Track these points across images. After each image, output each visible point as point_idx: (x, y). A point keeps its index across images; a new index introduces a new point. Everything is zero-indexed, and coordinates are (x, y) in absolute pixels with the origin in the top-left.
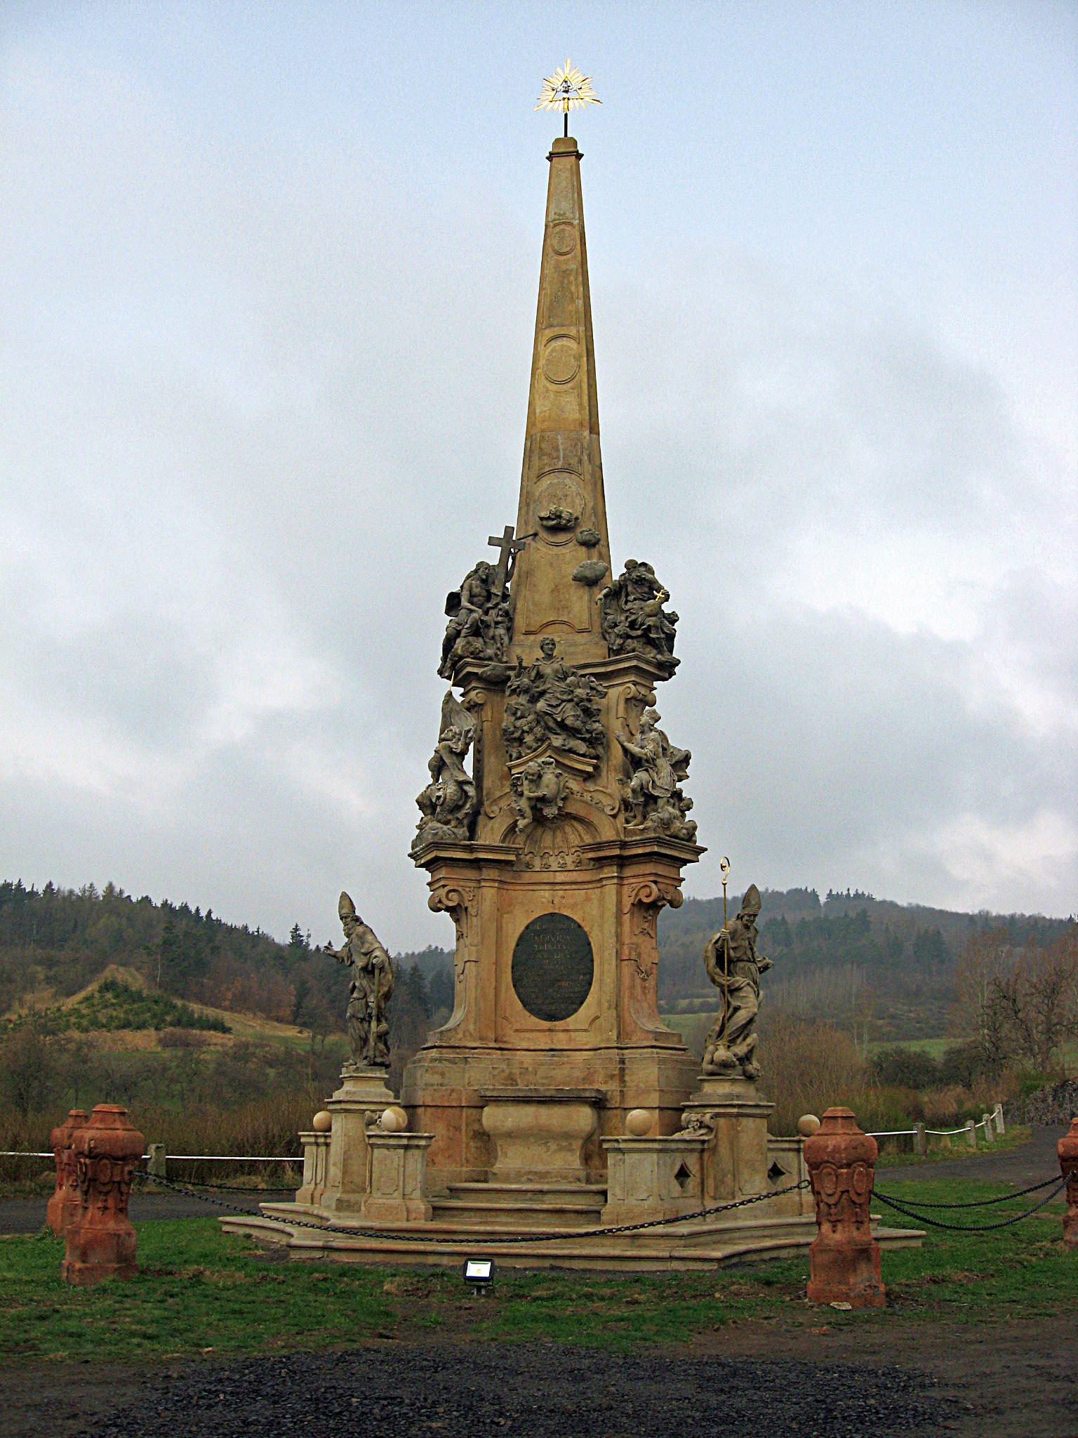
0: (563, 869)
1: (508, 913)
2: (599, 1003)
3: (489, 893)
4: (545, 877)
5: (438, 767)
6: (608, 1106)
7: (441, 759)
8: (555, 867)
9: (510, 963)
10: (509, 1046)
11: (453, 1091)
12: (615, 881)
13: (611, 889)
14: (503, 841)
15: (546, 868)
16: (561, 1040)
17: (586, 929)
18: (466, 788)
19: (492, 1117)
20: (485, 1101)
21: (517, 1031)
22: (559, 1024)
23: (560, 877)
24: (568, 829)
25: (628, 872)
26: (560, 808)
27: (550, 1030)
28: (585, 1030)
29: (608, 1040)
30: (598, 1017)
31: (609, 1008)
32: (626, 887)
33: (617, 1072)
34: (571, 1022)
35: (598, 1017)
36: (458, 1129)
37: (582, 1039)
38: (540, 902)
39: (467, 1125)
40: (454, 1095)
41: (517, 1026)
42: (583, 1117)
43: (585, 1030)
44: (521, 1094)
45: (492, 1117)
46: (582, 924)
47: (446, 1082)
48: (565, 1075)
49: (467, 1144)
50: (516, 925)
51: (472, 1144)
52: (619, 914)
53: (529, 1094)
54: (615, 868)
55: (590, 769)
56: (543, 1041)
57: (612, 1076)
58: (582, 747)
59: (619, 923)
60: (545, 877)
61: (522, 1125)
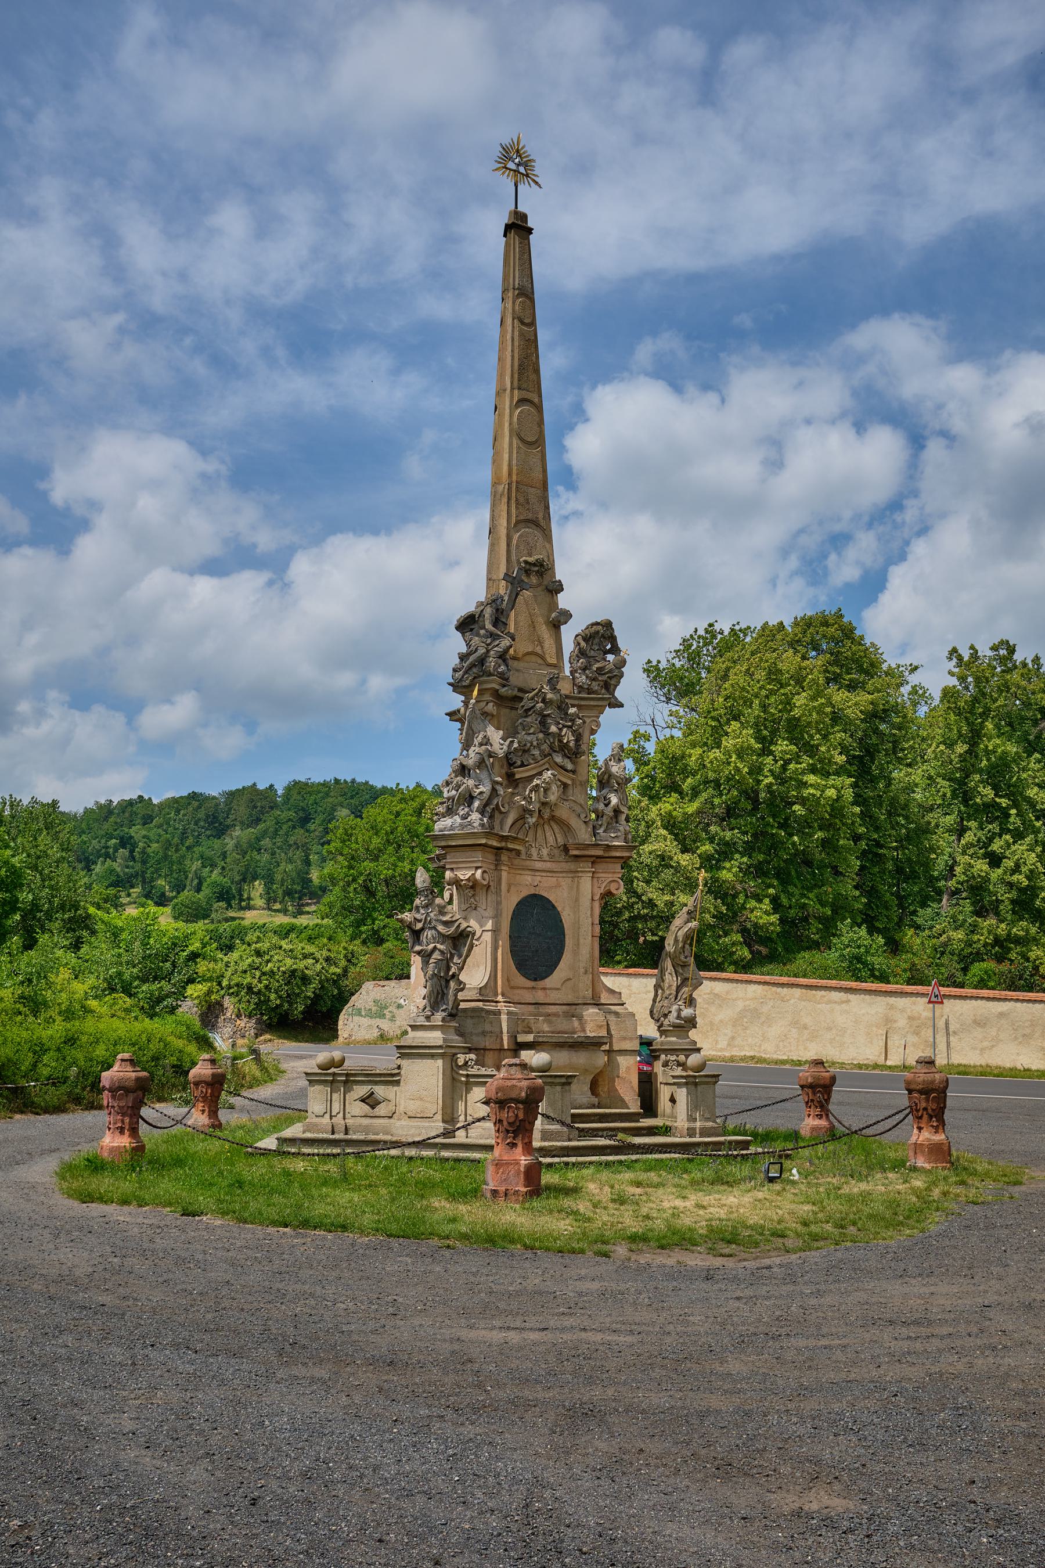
0: (541, 860)
16: (540, 996)
17: (559, 909)
22: (541, 984)
28: (558, 989)
34: (549, 982)
37: (553, 997)
56: (528, 997)
57: (601, 1027)
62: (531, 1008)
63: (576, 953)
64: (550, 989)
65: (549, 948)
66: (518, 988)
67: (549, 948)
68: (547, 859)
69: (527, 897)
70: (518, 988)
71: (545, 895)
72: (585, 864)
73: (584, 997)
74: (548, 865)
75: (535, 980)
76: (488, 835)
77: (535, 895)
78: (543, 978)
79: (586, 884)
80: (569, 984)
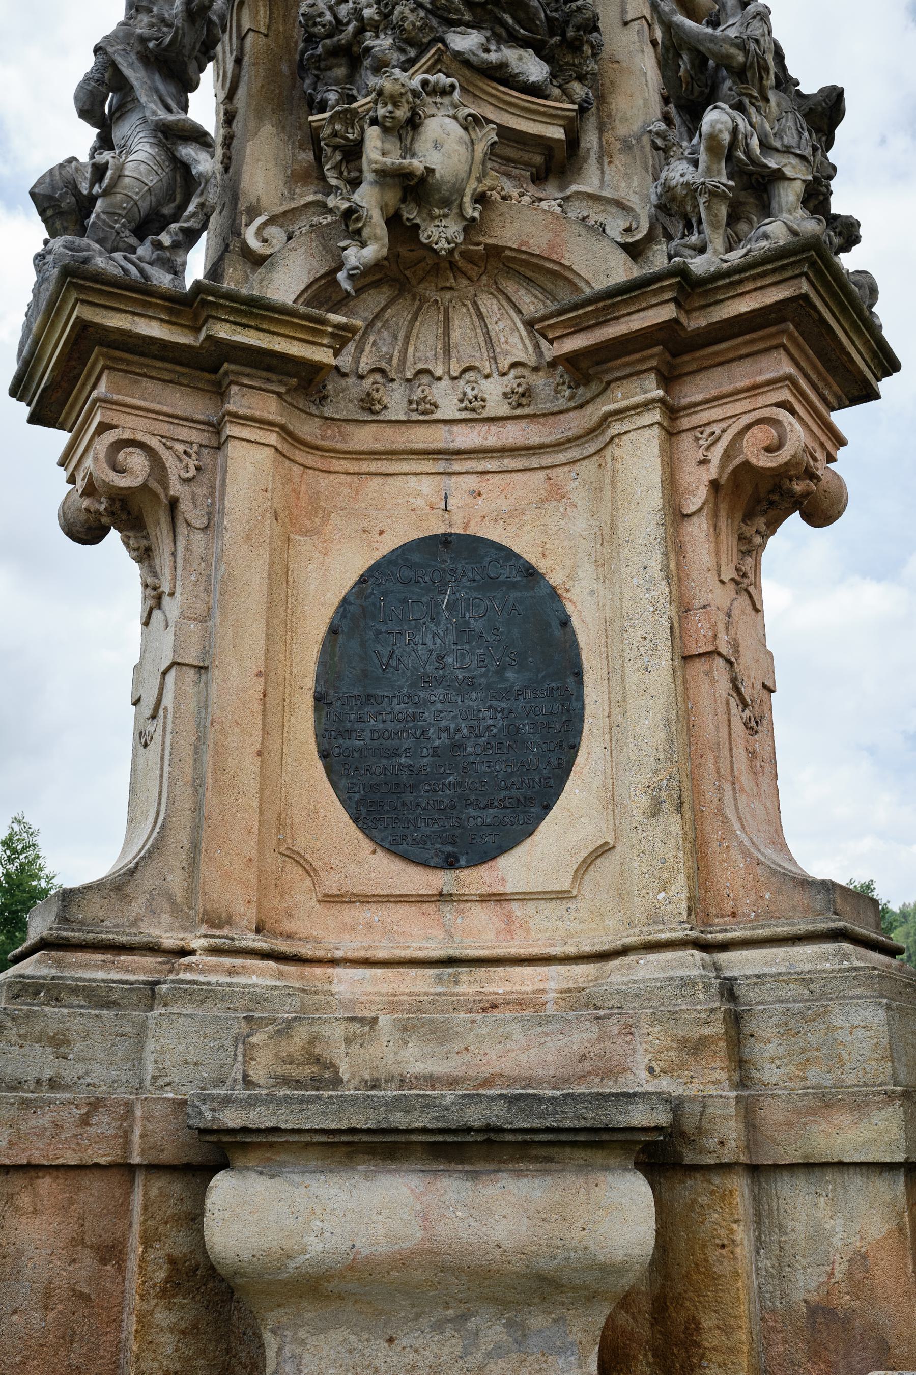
0: (474, 413)
1: (307, 533)
2: (611, 801)
3: (249, 466)
4: (421, 437)
5: (103, 98)
6: (689, 1158)
7: (114, 65)
8: (449, 408)
9: (309, 682)
10: (306, 950)
11: (95, 1105)
12: (655, 416)
13: (640, 452)
14: (295, 302)
15: (423, 413)
16: (479, 931)
17: (556, 579)
18: (188, 152)
19: (247, 1215)
20: (216, 1151)
21: (330, 900)
22: (477, 879)
23: (466, 437)
24: (489, 305)
25: (693, 391)
26: (471, 226)
27: (442, 897)
28: (561, 896)
29: (654, 918)
30: (604, 850)
31: (655, 811)
32: (686, 441)
33: (717, 1028)
34: (514, 869)
35: (604, 850)
36: (111, 1253)
37: (543, 930)
38: (407, 507)
39: (147, 1241)
40: (103, 1124)
41: (331, 884)
42: (618, 1215)
43: (561, 896)
44: (358, 1120)
45: (247, 1215)
46: (542, 566)
47: (70, 1071)
48: (515, 1052)
49: (143, 1319)
50: (333, 571)
51: (162, 1317)
52: (676, 516)
53: (399, 1120)
54: (651, 380)
55: (557, 133)
56: (423, 935)
57: (696, 1048)
58: (534, 69)
59: (675, 547)
60: (421, 437)
61: (365, 1248)
62: (420, 982)
63: (615, 733)
64: (524, 897)
65: (513, 732)
66: (365, 899)
67: (513, 732)
68: (504, 410)
69: (406, 548)
70: (365, 899)
71: (495, 534)
72: (631, 385)
73: (654, 918)
74: (512, 434)
75: (450, 863)
76: (900, 970)
77: (445, 540)
78: (486, 855)
79: (640, 452)
80: (607, 867)
